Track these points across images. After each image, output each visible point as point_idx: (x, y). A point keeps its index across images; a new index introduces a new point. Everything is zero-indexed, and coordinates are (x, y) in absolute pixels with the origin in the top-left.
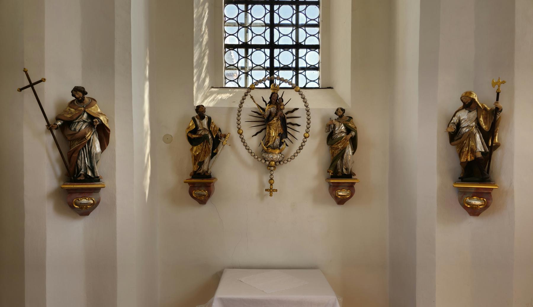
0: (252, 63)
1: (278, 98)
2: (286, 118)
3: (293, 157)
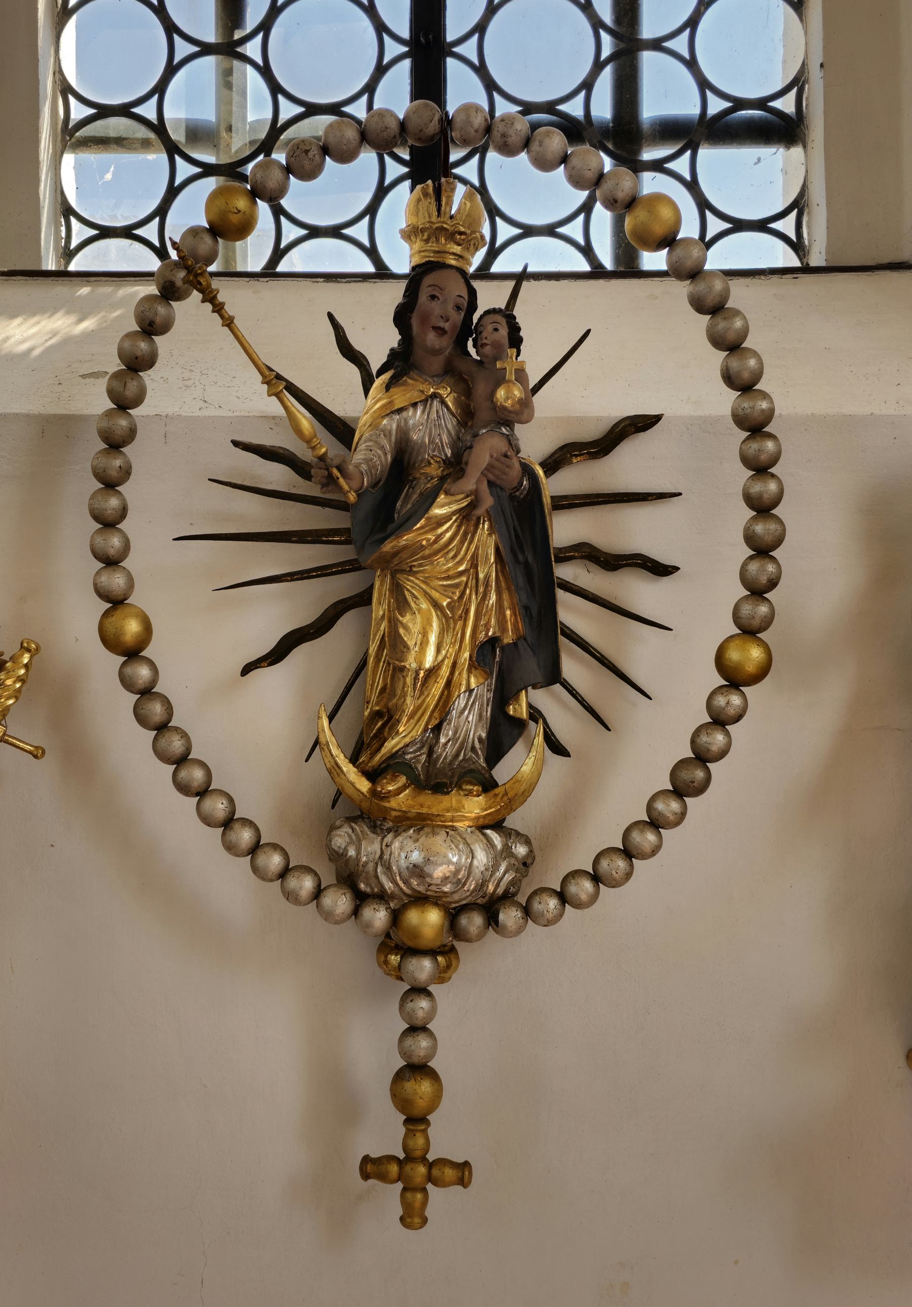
0: (276, 89)
1: (476, 317)
2: (547, 501)
3: (621, 863)
